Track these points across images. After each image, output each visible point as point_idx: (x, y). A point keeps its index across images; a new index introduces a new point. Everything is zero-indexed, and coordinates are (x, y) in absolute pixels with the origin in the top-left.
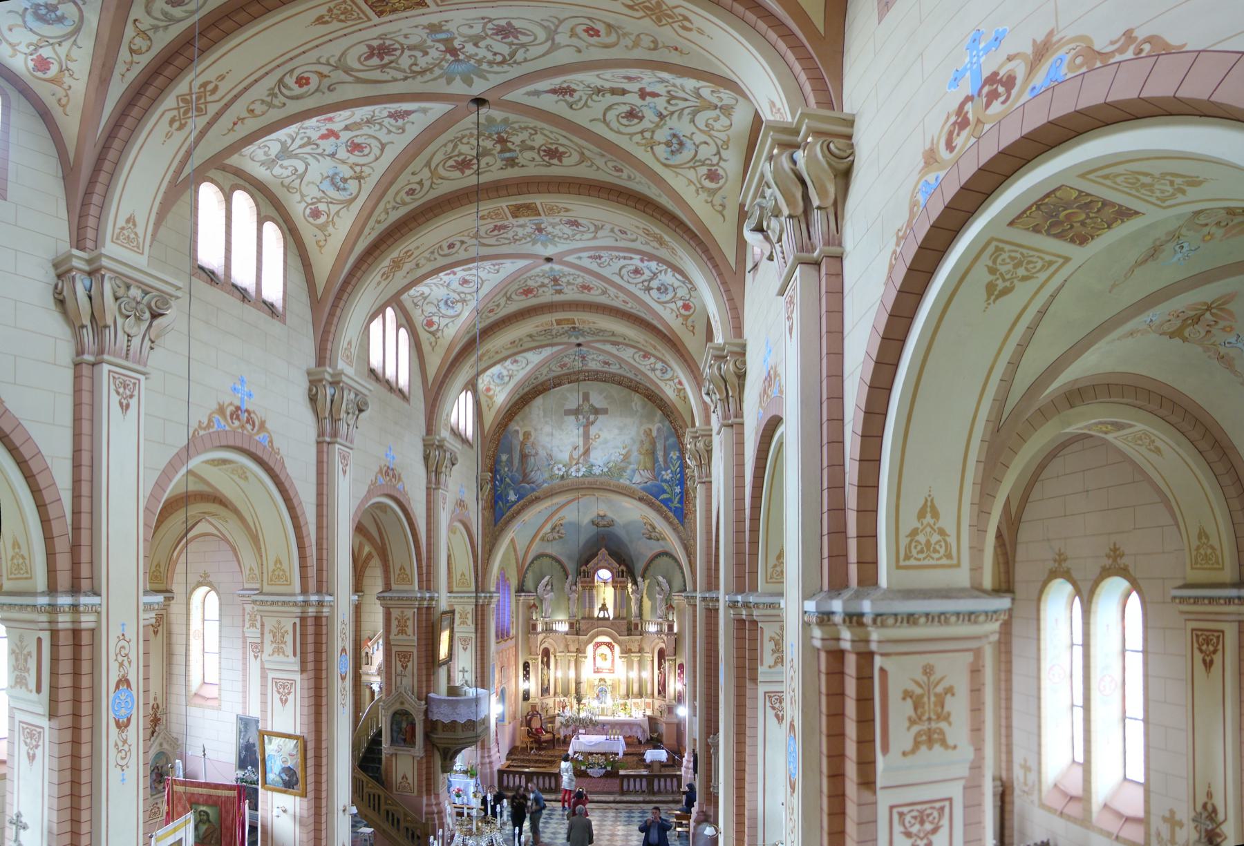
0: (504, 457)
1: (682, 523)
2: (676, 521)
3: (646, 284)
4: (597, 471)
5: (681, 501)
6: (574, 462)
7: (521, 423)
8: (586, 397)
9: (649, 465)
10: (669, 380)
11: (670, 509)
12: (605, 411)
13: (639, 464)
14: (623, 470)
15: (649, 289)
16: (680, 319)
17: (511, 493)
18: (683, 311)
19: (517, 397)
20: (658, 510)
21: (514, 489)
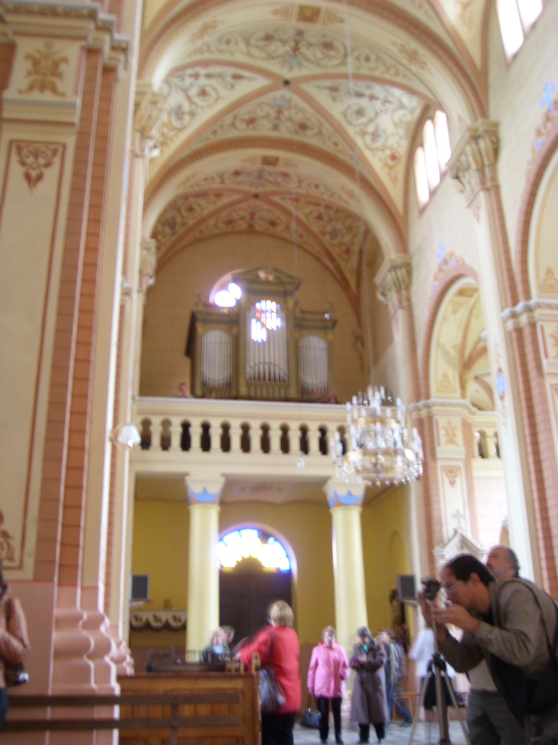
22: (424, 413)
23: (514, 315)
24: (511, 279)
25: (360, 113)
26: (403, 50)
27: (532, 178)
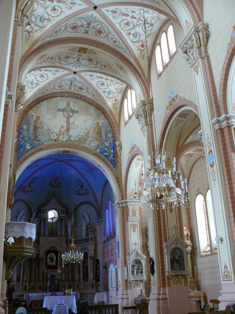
0: (25, 127)
1: (115, 167)
2: (112, 166)
3: (129, 31)
4: (72, 139)
5: (114, 157)
6: (62, 134)
7: (35, 112)
8: (68, 104)
9: (98, 139)
10: (111, 98)
11: (109, 160)
12: (77, 112)
13: (94, 137)
14: (86, 140)
15: (129, 34)
16: (139, 51)
17: (28, 145)
18: (141, 48)
19: (35, 98)
20: (103, 160)
21: (29, 143)
22: (224, 124)
23: (218, 122)
24: (216, 103)
25: (103, 84)
26: (118, 65)
27: (165, 124)
